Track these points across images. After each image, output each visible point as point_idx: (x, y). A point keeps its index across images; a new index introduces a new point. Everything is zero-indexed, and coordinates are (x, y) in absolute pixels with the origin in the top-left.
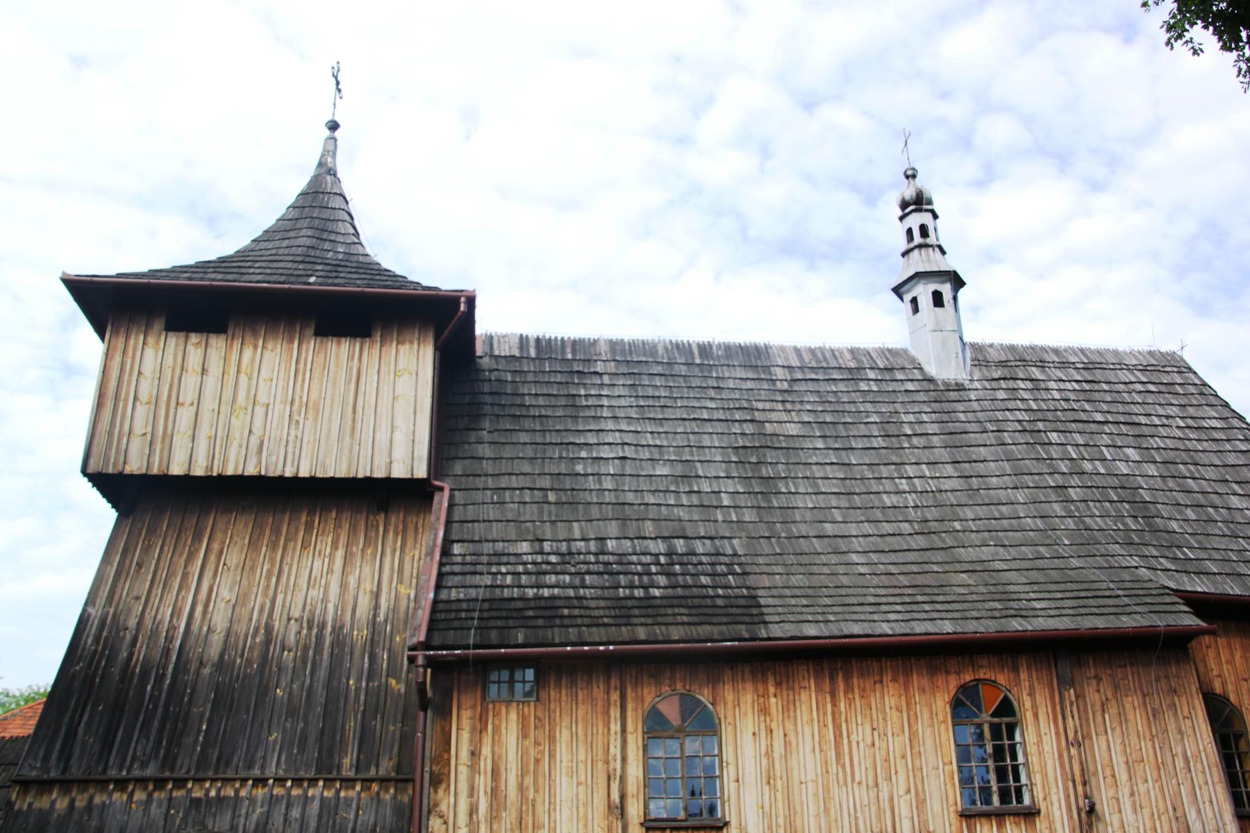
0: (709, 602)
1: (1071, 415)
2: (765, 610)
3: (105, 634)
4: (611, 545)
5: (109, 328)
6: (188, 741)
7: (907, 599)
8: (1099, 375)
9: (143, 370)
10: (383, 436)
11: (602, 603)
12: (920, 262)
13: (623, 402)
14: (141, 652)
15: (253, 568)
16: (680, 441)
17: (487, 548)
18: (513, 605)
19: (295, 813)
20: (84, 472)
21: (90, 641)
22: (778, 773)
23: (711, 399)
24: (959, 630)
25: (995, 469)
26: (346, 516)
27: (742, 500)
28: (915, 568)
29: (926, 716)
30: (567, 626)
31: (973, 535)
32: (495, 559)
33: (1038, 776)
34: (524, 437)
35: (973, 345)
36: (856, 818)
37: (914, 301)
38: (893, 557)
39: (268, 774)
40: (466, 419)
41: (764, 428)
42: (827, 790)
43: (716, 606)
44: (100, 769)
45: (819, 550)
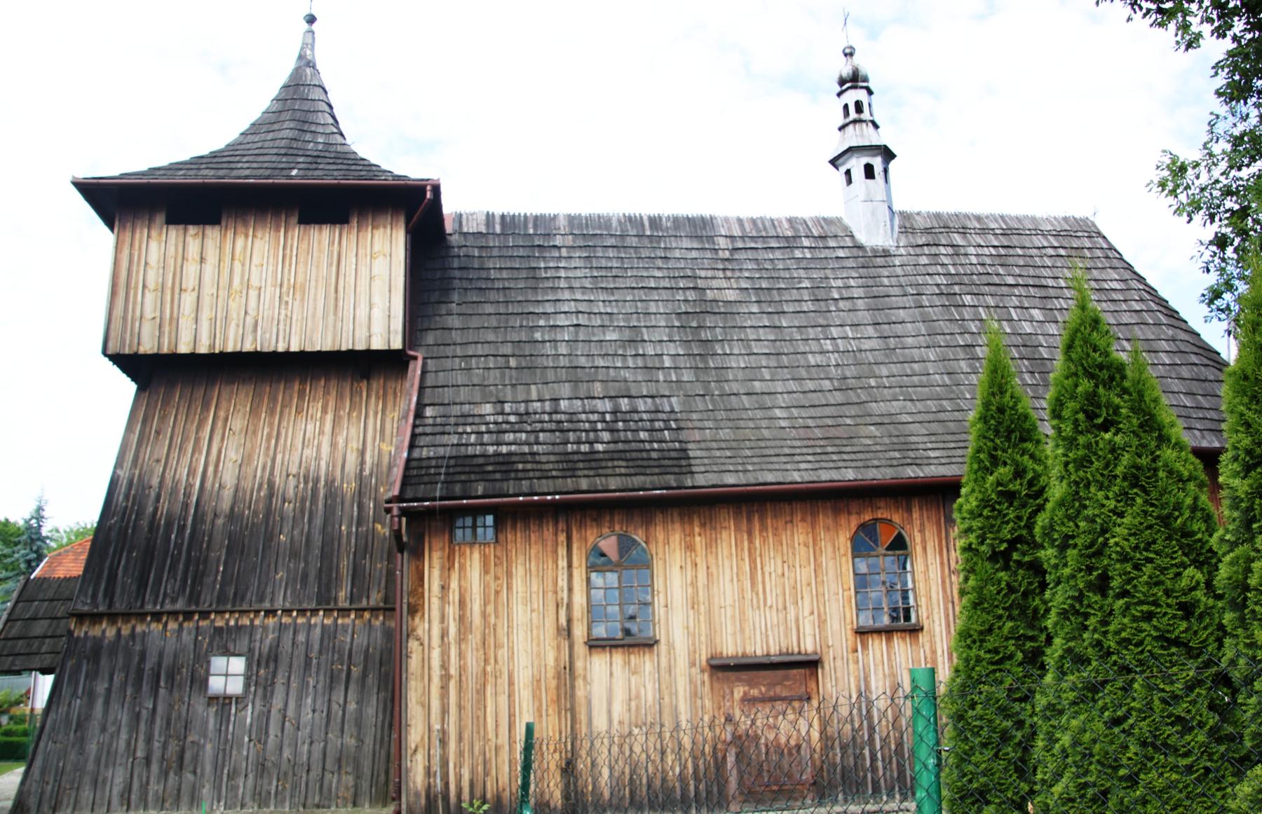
0: (645, 455)
1: (985, 279)
2: (693, 462)
3: (133, 492)
4: (563, 405)
5: (117, 224)
6: (208, 580)
7: (819, 450)
8: (1015, 240)
9: (149, 260)
10: (362, 313)
11: (552, 458)
12: (855, 137)
13: (579, 273)
14: (164, 506)
15: (255, 432)
16: (629, 308)
17: (456, 410)
18: (476, 461)
19: (301, 638)
20: (105, 353)
21: (121, 498)
22: (701, 599)
23: (659, 268)
24: (860, 477)
25: (911, 330)
26: (333, 383)
27: (682, 362)
28: (829, 421)
29: (830, 550)
30: (521, 479)
31: (886, 391)
32: (461, 420)
33: (923, 599)
34: (489, 309)
35: (901, 213)
36: (767, 636)
37: (848, 173)
38: (812, 412)
39: (276, 606)
40: (437, 293)
41: (705, 294)
42: (742, 613)
43: (651, 459)
44: (139, 604)
45: (747, 406)
